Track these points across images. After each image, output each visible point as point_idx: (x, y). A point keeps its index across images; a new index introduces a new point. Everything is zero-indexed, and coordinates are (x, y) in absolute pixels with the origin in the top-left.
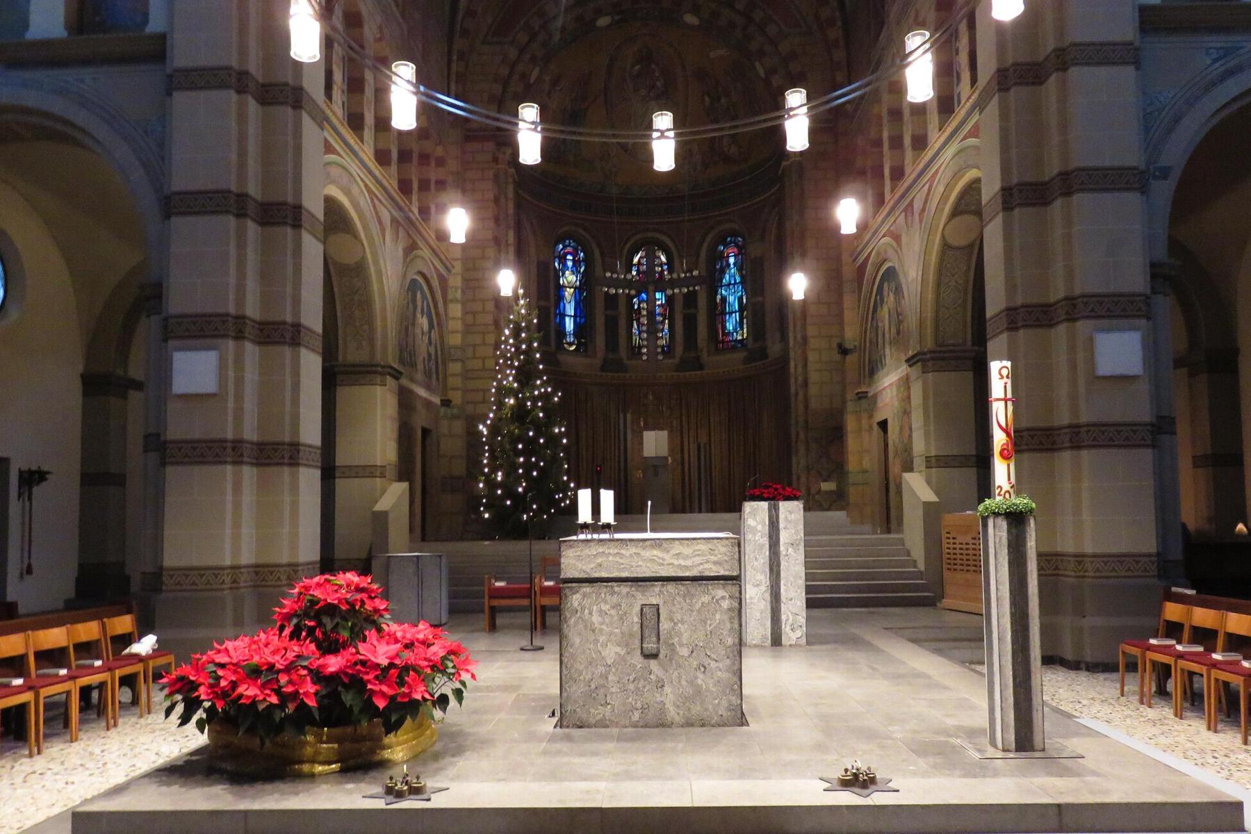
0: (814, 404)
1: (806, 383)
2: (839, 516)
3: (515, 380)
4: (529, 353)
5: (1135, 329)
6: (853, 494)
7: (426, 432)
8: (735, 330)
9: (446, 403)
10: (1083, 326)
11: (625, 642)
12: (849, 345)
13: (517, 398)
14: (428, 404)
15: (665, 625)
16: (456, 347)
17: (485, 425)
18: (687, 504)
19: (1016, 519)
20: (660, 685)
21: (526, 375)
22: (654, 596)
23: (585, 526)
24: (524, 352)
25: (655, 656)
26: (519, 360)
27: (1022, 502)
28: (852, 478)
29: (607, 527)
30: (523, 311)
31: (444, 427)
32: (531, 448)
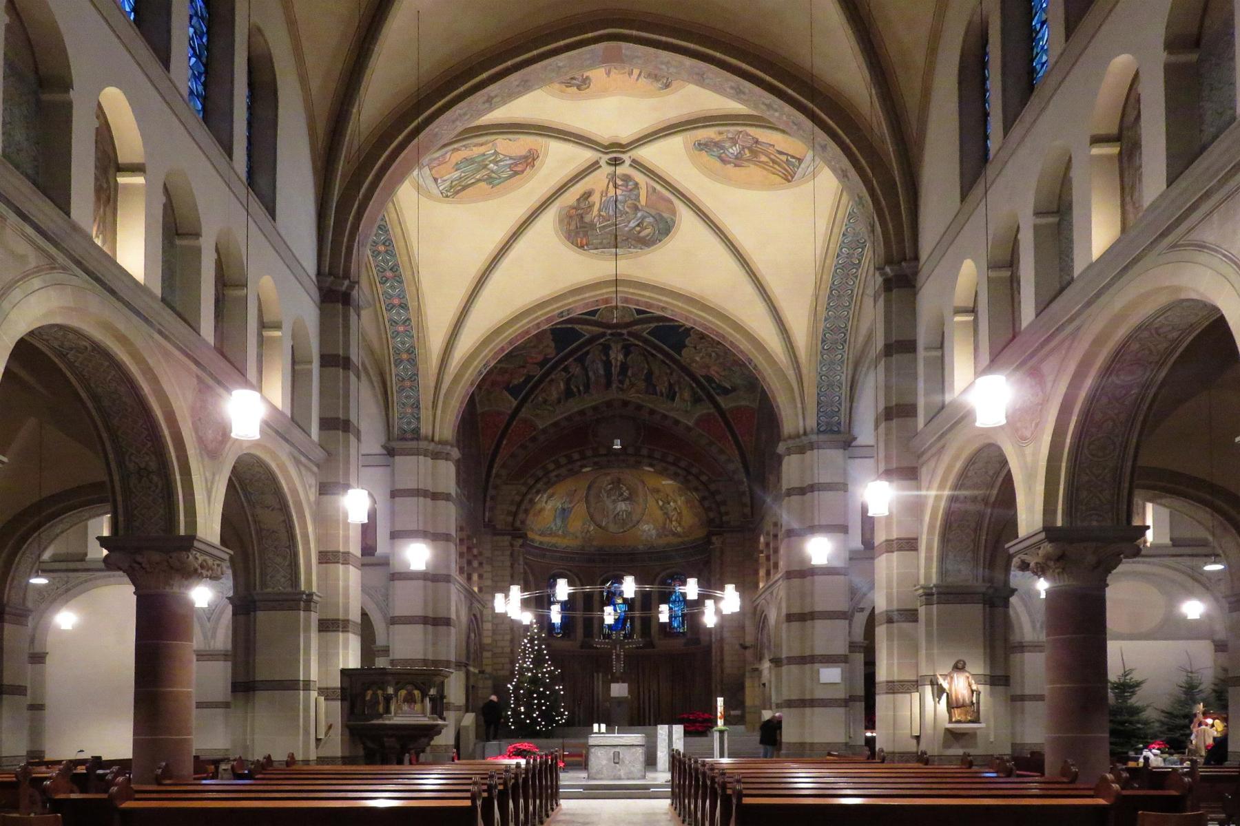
0: (728, 670)
1: (722, 661)
2: (741, 728)
3: (531, 663)
4: (540, 650)
5: (838, 667)
6: (748, 717)
7: (473, 687)
8: (679, 626)
9: (482, 672)
10: (817, 666)
11: (609, 760)
12: (747, 644)
13: (532, 672)
14: (474, 674)
15: (621, 756)
16: (487, 645)
17: (511, 684)
18: (647, 721)
19: (721, 732)
20: (620, 770)
21: (538, 661)
22: (617, 749)
23: (596, 733)
24: (537, 650)
25: (618, 763)
26: (534, 654)
27: (723, 728)
28: (747, 710)
29: (603, 733)
30: (536, 631)
31: (480, 684)
32: (541, 696)
